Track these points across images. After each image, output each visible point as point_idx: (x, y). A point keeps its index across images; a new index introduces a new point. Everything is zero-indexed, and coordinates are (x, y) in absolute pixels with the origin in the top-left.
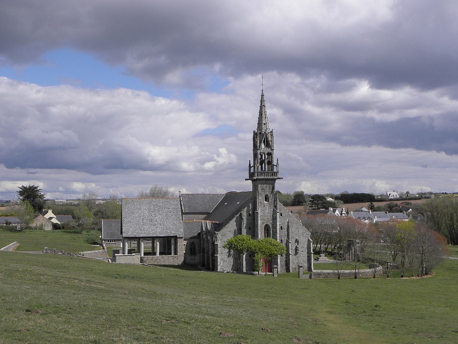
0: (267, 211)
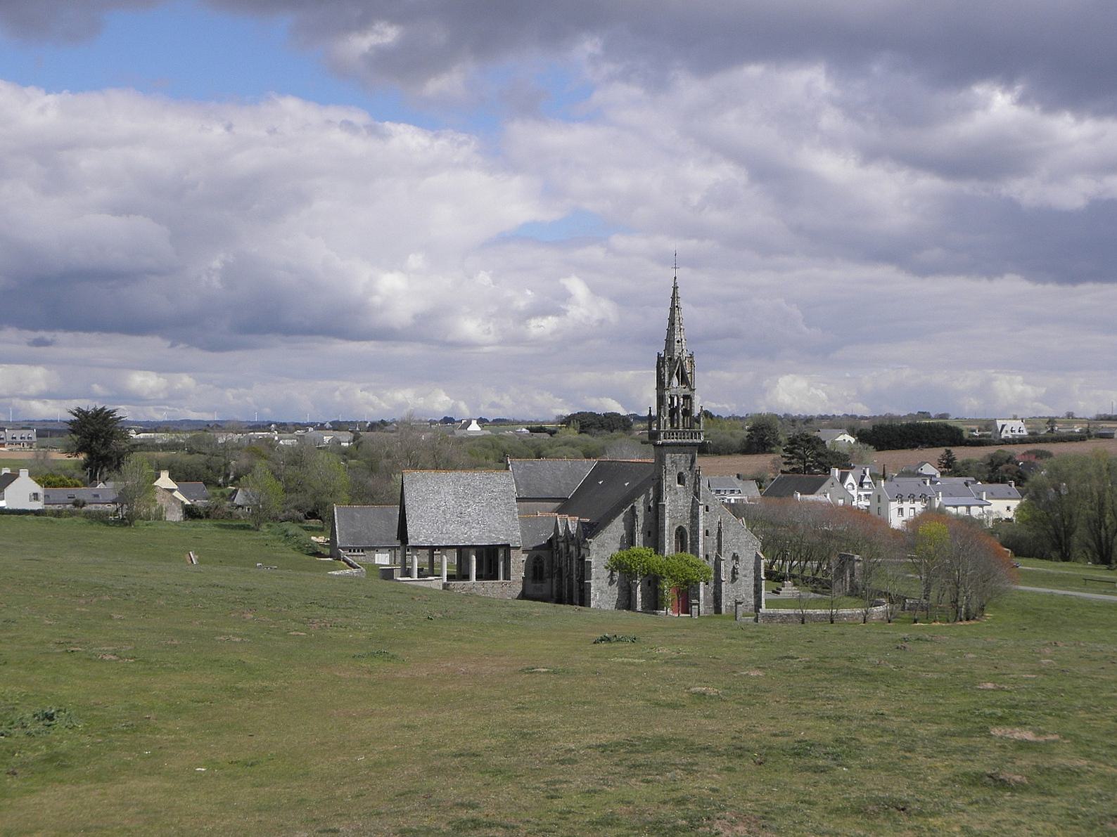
0: (680, 503)
